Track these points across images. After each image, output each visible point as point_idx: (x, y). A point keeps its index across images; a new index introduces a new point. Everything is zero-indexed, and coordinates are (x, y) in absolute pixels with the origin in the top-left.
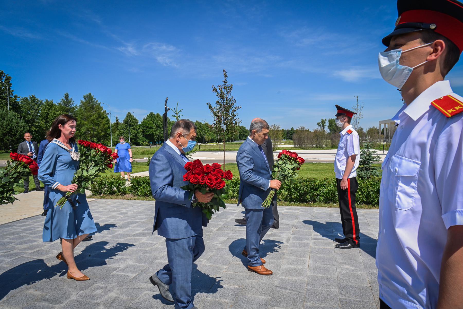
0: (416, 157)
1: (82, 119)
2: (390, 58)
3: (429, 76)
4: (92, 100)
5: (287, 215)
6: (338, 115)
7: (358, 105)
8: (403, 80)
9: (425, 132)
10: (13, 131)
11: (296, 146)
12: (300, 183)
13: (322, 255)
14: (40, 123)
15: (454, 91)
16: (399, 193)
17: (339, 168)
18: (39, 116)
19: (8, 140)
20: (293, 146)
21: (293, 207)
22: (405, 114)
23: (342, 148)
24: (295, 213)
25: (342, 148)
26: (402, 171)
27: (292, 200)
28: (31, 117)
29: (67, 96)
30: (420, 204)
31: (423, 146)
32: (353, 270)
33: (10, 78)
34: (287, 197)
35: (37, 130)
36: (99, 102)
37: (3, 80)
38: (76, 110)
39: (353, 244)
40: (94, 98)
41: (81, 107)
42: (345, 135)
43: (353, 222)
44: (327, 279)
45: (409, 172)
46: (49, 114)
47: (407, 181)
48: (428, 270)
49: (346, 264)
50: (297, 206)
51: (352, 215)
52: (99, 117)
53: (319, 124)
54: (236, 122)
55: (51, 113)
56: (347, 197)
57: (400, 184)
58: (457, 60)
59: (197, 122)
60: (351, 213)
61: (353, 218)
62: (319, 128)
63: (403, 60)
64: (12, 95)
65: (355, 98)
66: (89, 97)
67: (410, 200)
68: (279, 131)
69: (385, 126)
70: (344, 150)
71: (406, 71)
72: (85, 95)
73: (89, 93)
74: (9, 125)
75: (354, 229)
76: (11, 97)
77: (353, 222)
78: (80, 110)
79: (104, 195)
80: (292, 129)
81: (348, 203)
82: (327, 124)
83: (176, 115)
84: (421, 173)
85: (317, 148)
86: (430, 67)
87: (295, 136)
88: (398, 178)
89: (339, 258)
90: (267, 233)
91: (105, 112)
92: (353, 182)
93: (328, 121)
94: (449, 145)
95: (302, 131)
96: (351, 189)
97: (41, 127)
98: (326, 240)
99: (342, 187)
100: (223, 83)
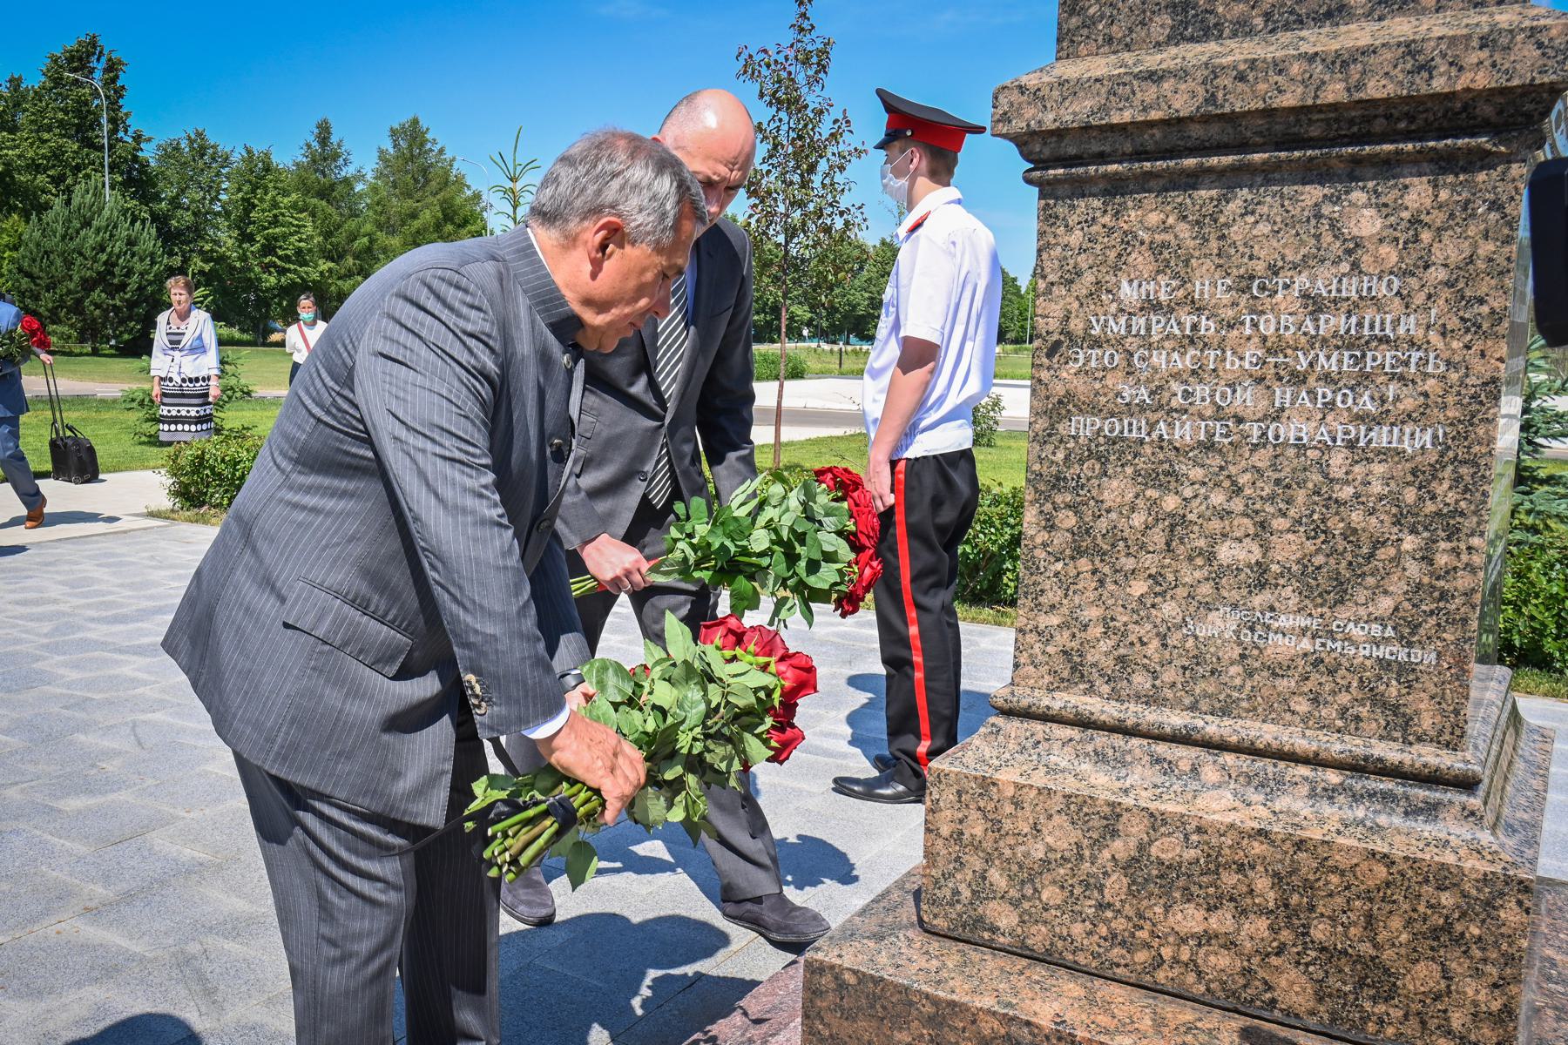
1: (380, 226)
4: (422, 145)
10: (117, 270)
14: (216, 242)
18: (218, 214)
19: (97, 306)
28: (188, 217)
29: (324, 133)
33: (120, 63)
35: (207, 268)
36: (448, 155)
37: (98, 75)
38: (359, 187)
40: (428, 136)
41: (380, 175)
46: (254, 206)
52: (448, 218)
54: (847, 223)
55: (262, 200)
59: (883, 243)
64: (126, 132)
66: (412, 137)
72: (396, 126)
73: (411, 117)
74: (103, 250)
76: (121, 140)
78: (375, 189)
79: (213, 511)
83: (509, 184)
90: (171, 617)
91: (477, 197)
97: (222, 259)
100: (791, 36)
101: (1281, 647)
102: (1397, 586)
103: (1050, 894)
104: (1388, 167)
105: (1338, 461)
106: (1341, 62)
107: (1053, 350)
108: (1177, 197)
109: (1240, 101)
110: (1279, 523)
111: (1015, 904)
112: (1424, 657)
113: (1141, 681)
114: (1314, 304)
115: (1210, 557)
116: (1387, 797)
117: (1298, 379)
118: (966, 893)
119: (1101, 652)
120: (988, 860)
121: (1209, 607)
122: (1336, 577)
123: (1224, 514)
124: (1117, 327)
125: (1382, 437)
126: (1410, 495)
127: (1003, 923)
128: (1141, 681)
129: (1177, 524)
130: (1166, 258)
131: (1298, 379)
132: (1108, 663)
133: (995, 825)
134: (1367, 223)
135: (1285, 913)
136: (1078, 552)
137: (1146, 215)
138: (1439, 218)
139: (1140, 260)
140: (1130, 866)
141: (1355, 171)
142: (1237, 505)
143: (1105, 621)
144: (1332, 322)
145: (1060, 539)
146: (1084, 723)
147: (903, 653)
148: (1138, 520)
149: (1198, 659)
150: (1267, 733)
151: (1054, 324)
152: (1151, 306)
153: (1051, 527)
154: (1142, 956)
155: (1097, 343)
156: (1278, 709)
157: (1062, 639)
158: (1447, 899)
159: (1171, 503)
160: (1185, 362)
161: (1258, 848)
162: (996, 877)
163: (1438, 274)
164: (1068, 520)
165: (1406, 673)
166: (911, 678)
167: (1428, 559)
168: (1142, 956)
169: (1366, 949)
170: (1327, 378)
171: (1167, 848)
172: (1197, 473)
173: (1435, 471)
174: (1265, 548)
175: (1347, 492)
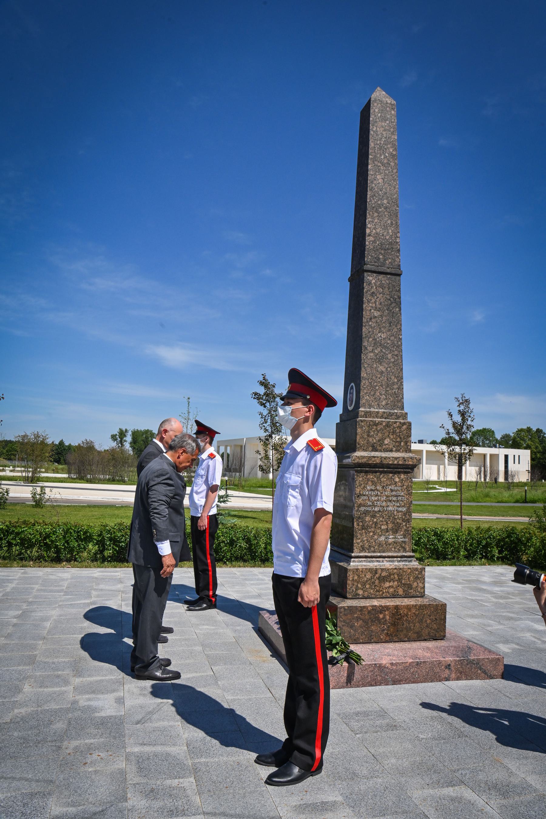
0: (299, 473)
2: (285, 411)
3: (306, 425)
5: (103, 579)
6: (198, 433)
7: (189, 413)
8: (292, 425)
9: (304, 459)
11: (72, 476)
12: (120, 530)
13: (172, 619)
15: (319, 436)
16: (289, 496)
17: (196, 501)
20: (66, 476)
21: (107, 569)
22: (293, 447)
23: (202, 476)
24: (116, 576)
25: (202, 476)
26: (291, 482)
27: (104, 560)
30: (301, 502)
31: (303, 466)
32: (214, 629)
34: (95, 554)
39: (209, 603)
42: (206, 459)
43: (210, 573)
44: (186, 639)
45: (296, 483)
47: (294, 488)
48: (304, 542)
49: (204, 625)
50: (115, 567)
51: (210, 564)
53: (114, 437)
56: (205, 540)
57: (290, 490)
58: (320, 416)
60: (209, 561)
61: (210, 569)
62: (114, 444)
63: (293, 413)
65: (186, 400)
67: (295, 500)
68: (47, 445)
69: (226, 449)
70: (204, 479)
71: (294, 421)
75: (211, 583)
77: (210, 573)
80: (61, 443)
81: (205, 547)
82: (129, 438)
84: (302, 483)
85: (112, 481)
86: (306, 420)
87: (71, 457)
88: (289, 487)
89: (194, 621)
92: (213, 520)
93: (130, 433)
94: (316, 467)
95: (88, 449)
96: (209, 530)
98: (172, 604)
99: (200, 527)
101: (390, 541)
102: (403, 530)
103: (367, 586)
104: (399, 473)
105: (395, 512)
106: (396, 458)
107: (358, 496)
108: (374, 474)
109: (385, 462)
110: (389, 522)
111: (362, 589)
112: (407, 540)
113: (372, 549)
114: (392, 491)
115: (381, 528)
116: (406, 560)
117: (390, 501)
118: (354, 590)
119: (366, 546)
120: (358, 583)
121: (381, 536)
122: (396, 529)
123: (382, 521)
124: (367, 493)
125: (400, 509)
126: (404, 517)
127: (360, 593)
128: (372, 549)
129: (376, 523)
130: (373, 483)
131: (390, 501)
132: (368, 547)
133: (359, 576)
134: (397, 480)
135: (399, 580)
136: (363, 529)
137: (371, 476)
138: (405, 479)
139: (370, 483)
140: (379, 578)
141: (395, 473)
142: (384, 520)
143: (367, 540)
144: (394, 493)
145: (360, 527)
146: (366, 557)
147: (205, 567)
148: (371, 523)
149: (380, 544)
150: (390, 554)
151: (358, 492)
152: (372, 490)
153: (358, 525)
154: (381, 593)
155: (364, 495)
156: (390, 551)
157: (361, 544)
158: (417, 572)
159: (375, 520)
160: (376, 499)
161: (395, 571)
162: (359, 586)
163: (405, 487)
164: (361, 524)
165: (404, 542)
166: (208, 575)
167: (406, 526)
168: (381, 593)
169: (409, 582)
170: (394, 501)
171: (384, 574)
172: (378, 515)
173: (406, 513)
174: (387, 526)
175: (396, 517)
